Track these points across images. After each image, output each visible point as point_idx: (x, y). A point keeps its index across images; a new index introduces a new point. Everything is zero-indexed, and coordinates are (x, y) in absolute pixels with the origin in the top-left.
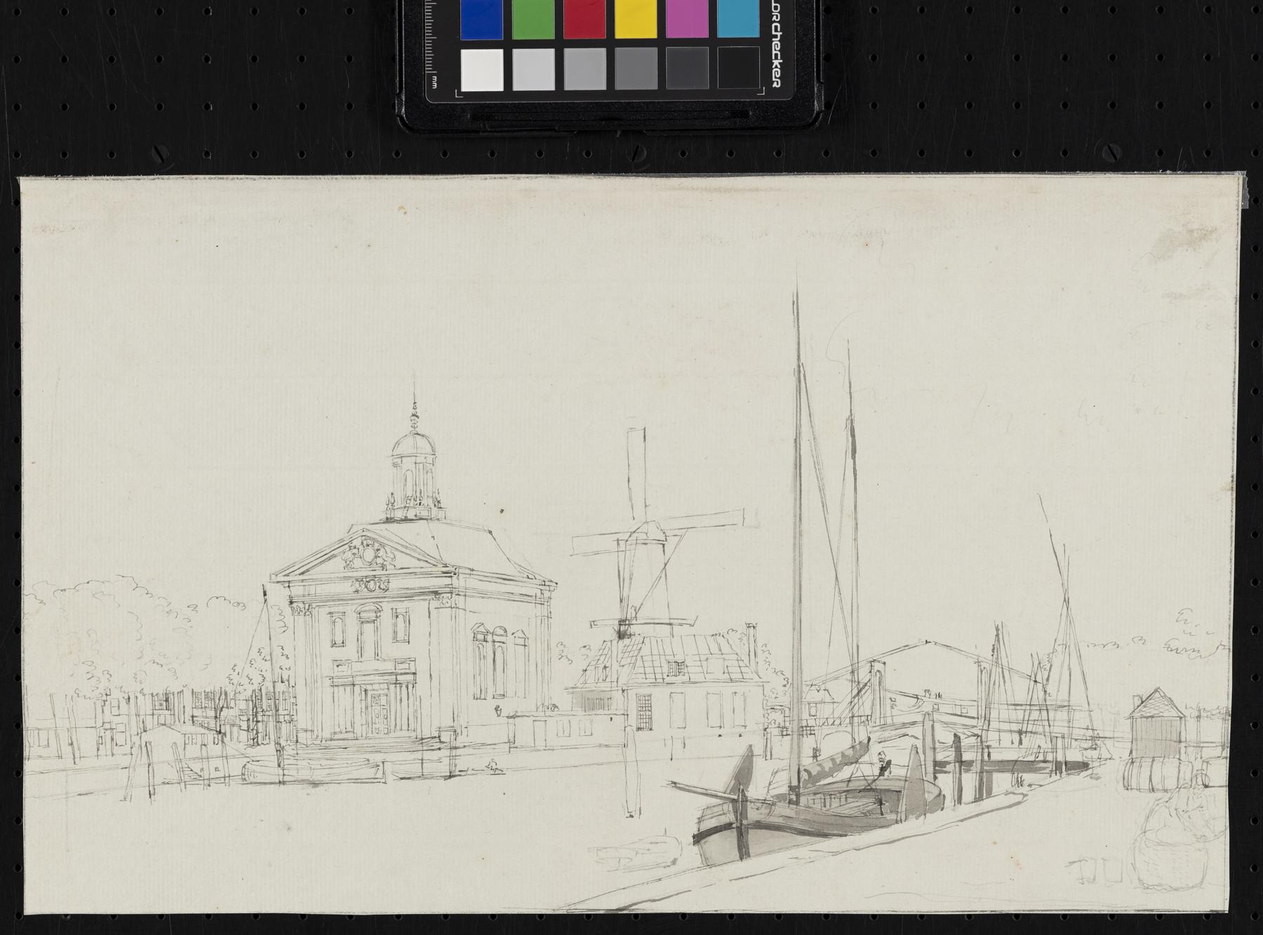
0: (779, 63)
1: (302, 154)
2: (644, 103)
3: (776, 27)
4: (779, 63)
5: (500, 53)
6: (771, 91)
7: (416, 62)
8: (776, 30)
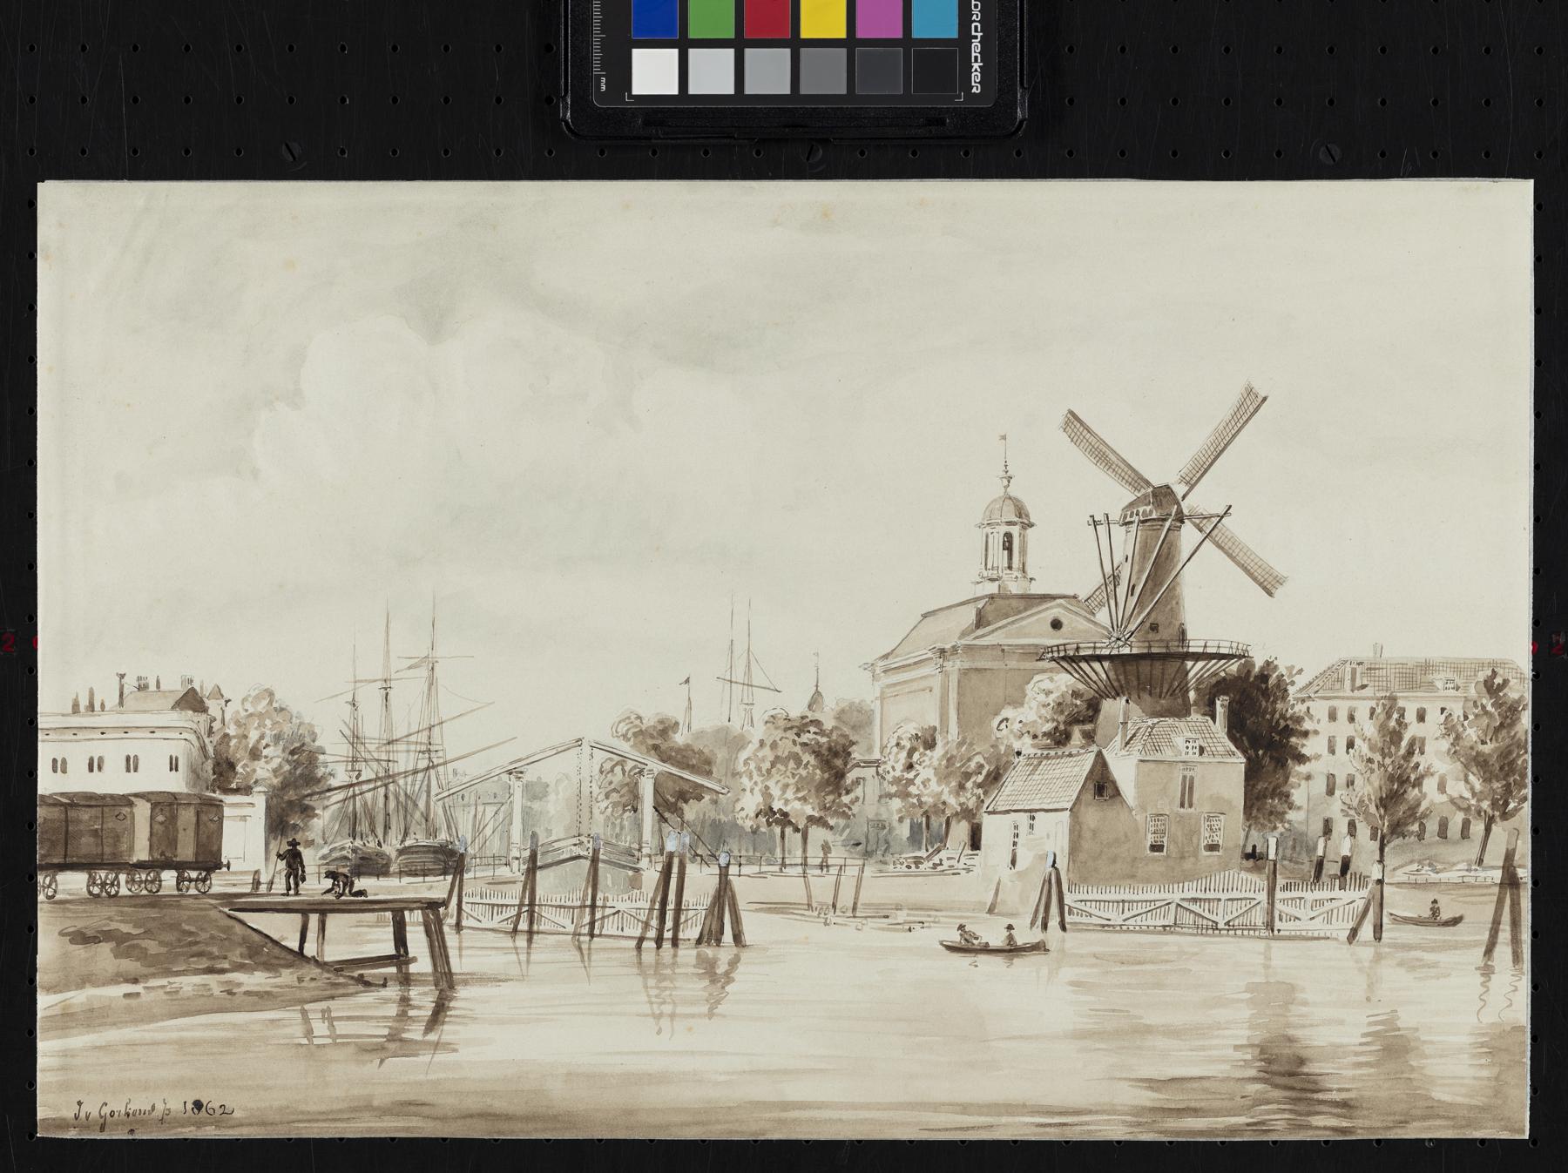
0: (980, 67)
1: (446, 152)
2: (832, 108)
3: (976, 27)
4: (980, 67)
5: (675, 52)
7: (583, 62)
8: (976, 31)
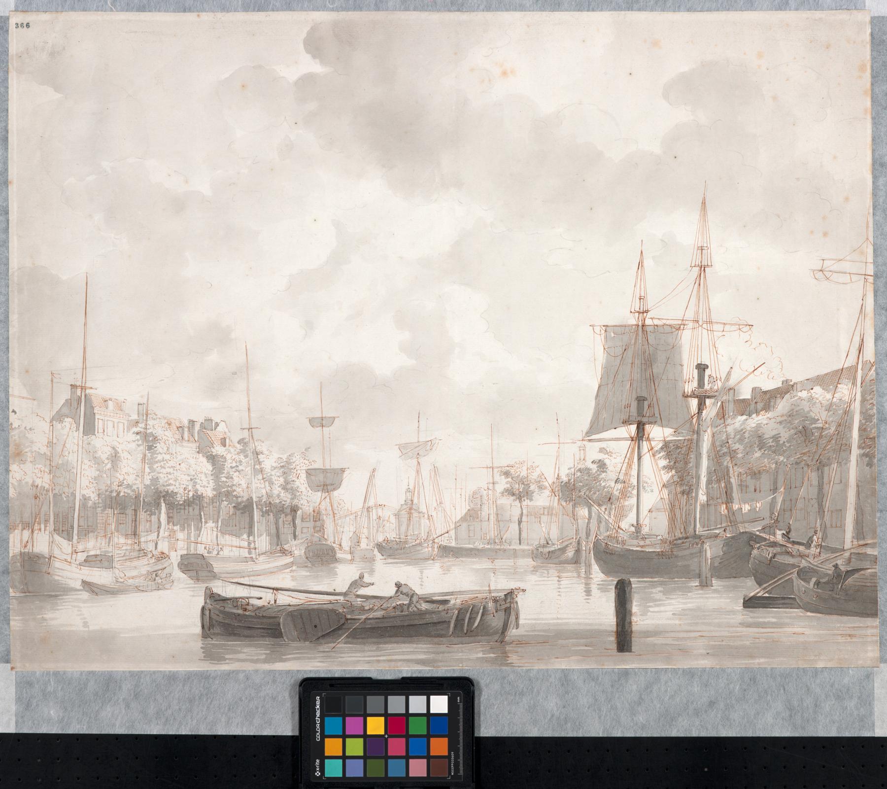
5: (432, 712)
6: (320, 695)
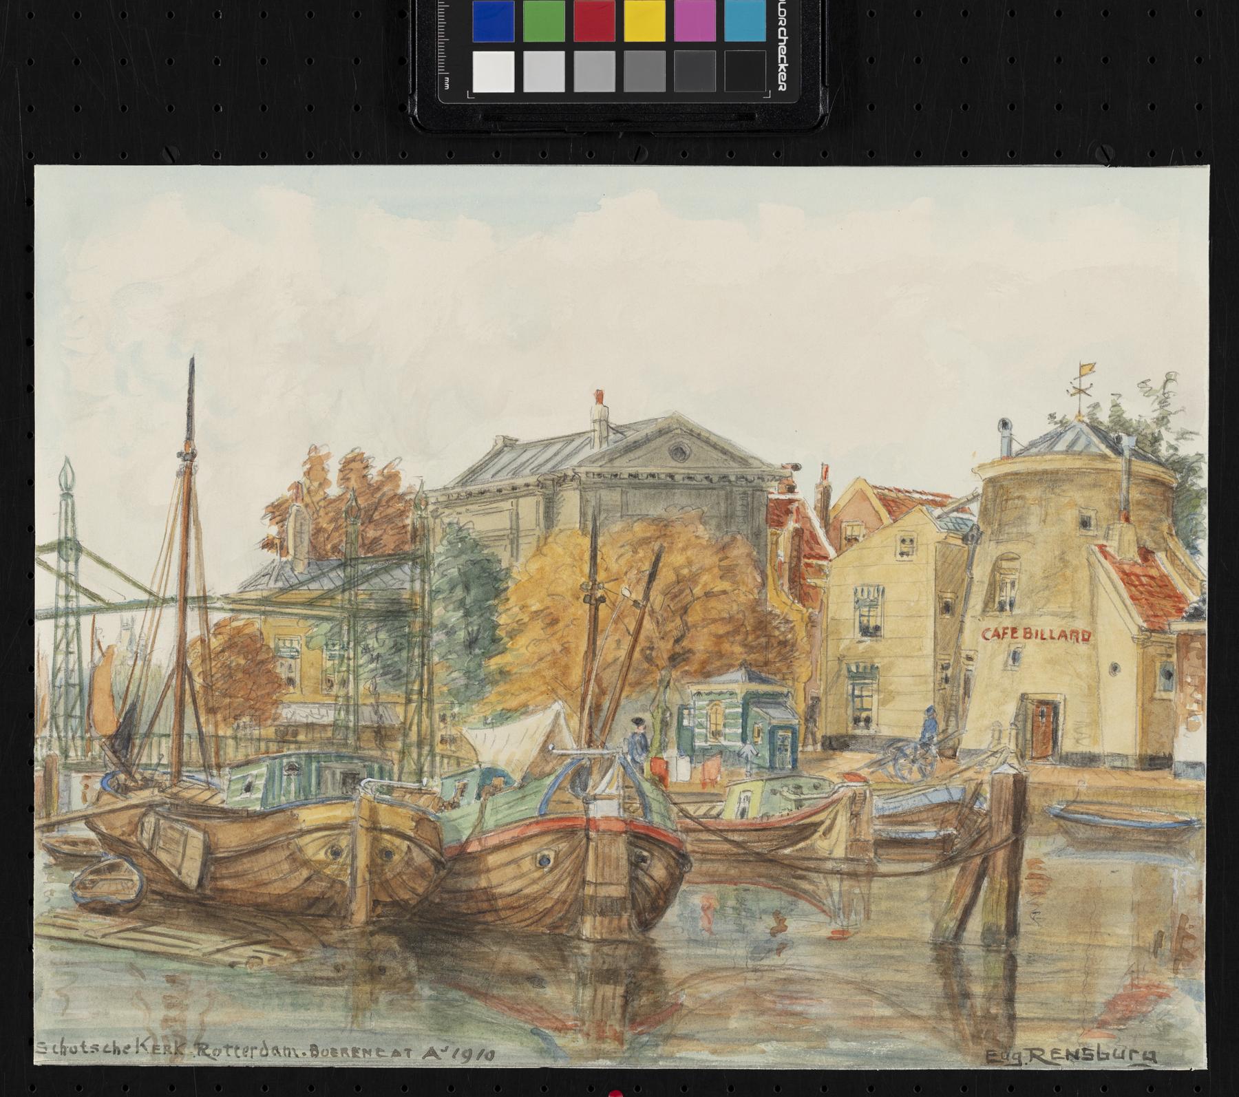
3: (782, 31)
5: (512, 54)
6: (777, 94)
8: (782, 35)
